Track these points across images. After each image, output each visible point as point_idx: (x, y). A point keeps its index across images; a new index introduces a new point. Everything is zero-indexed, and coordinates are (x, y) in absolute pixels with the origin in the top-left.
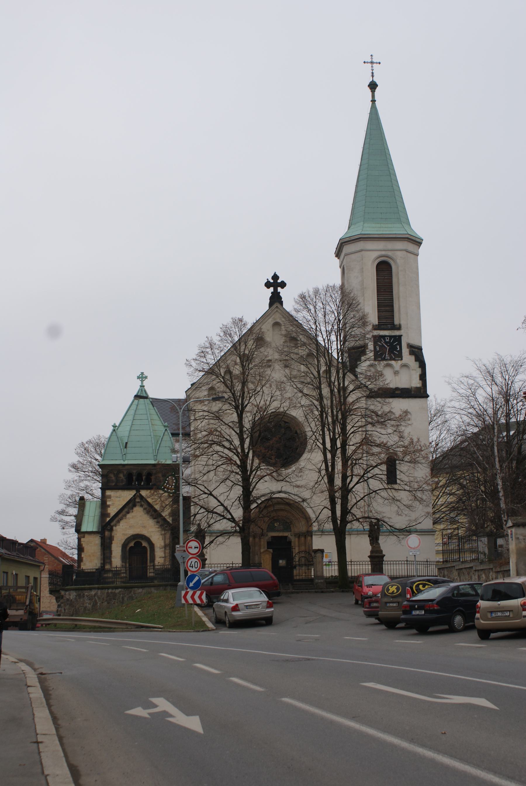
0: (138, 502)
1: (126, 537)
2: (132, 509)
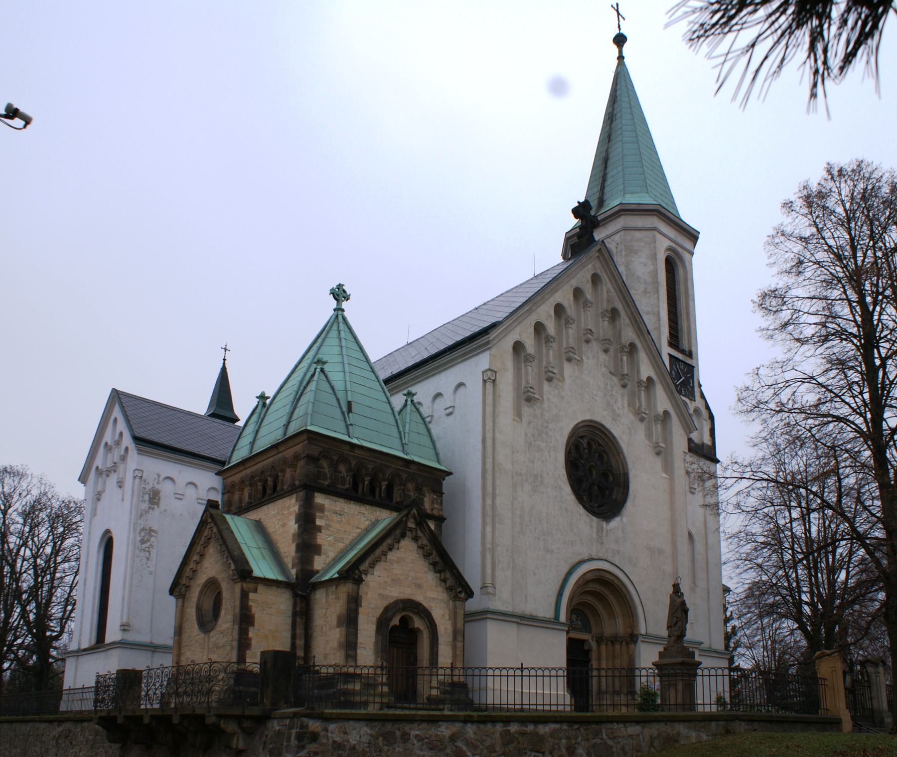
0: (411, 530)
1: (386, 603)
2: (399, 542)
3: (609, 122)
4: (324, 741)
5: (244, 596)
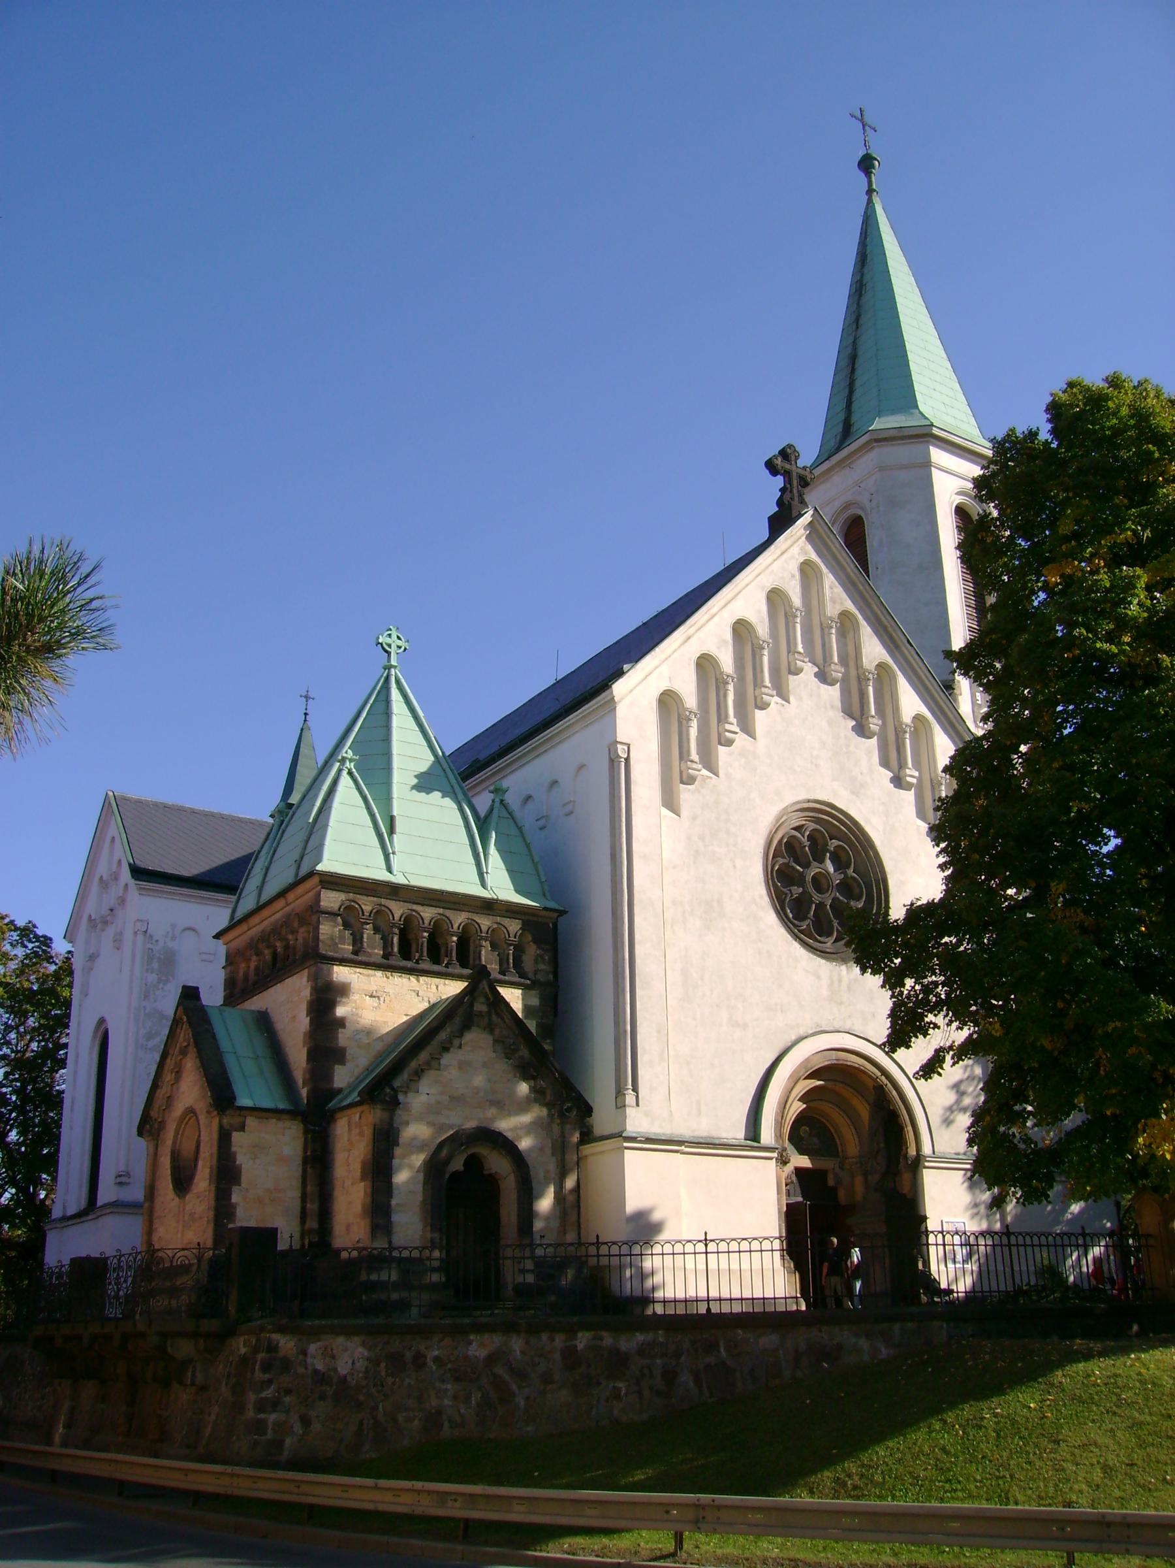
2: (461, 1036)
3: (856, 298)
4: (301, 1370)
5: (224, 1138)
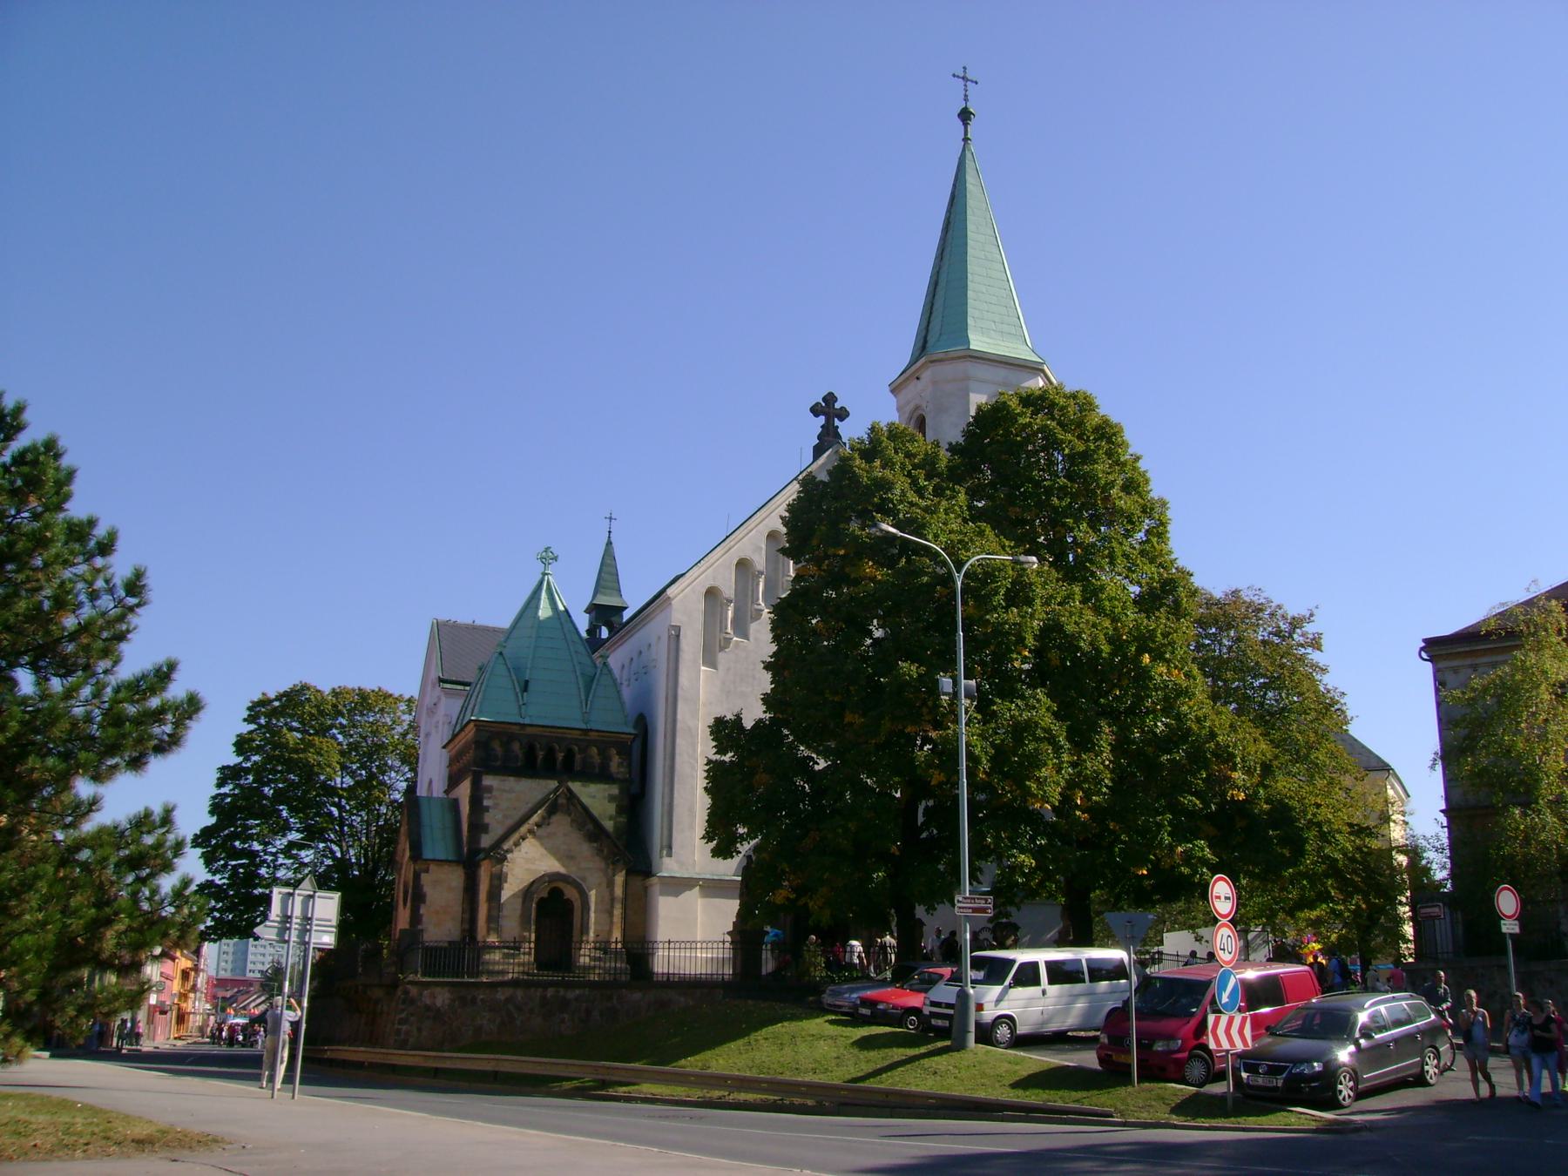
5: (417, 876)
